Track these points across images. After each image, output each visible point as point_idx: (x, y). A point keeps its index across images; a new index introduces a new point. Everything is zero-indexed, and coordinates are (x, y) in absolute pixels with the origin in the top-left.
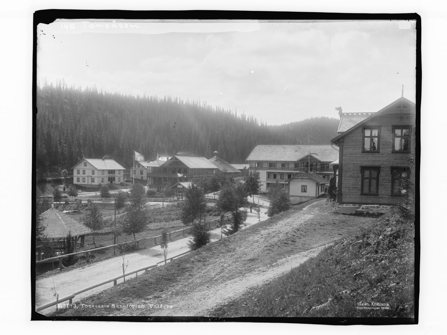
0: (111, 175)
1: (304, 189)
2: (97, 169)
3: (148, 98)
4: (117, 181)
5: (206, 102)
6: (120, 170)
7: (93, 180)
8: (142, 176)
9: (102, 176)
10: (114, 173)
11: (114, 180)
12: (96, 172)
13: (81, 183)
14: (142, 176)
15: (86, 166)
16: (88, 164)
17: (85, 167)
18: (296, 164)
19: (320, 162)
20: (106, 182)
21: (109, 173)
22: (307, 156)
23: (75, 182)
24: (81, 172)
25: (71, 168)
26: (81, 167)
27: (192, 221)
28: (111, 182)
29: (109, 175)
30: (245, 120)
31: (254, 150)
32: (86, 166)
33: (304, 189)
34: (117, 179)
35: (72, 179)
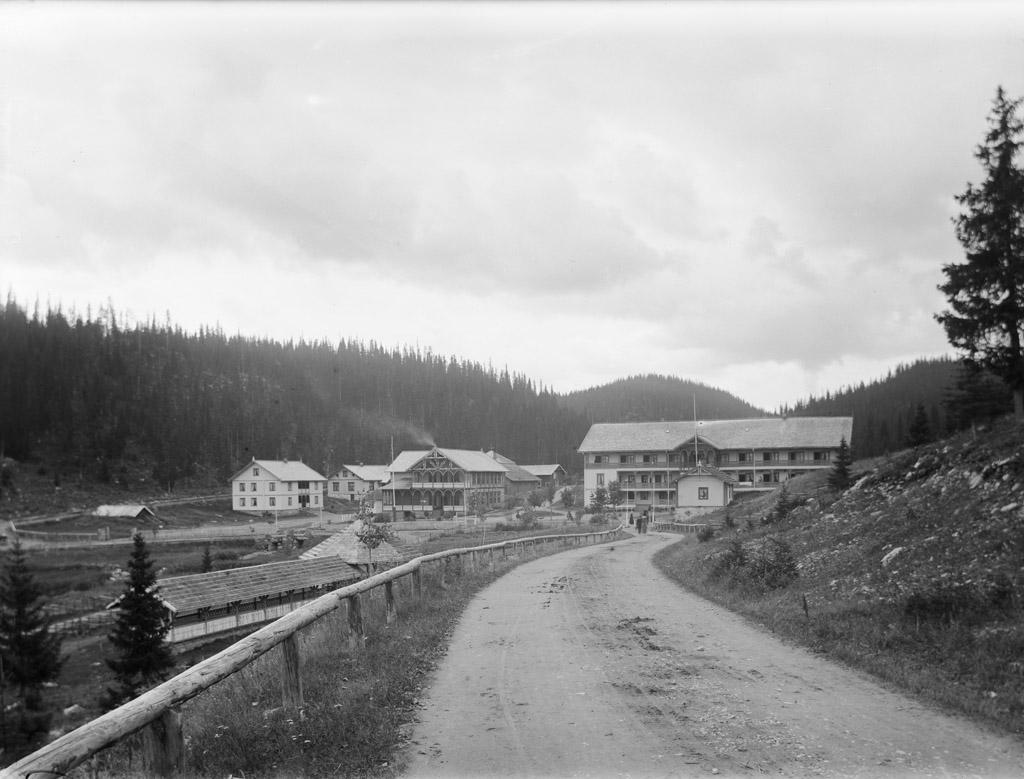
0: (304, 491)
1: (704, 494)
2: (279, 480)
3: (310, 346)
4: (312, 504)
5: (430, 348)
6: (316, 482)
7: (273, 502)
8: (352, 493)
9: (289, 493)
10: (308, 487)
11: (308, 501)
12: (278, 485)
13: (249, 507)
14: (352, 493)
15: (257, 474)
16: (261, 472)
17: (257, 478)
18: (671, 455)
19: (716, 450)
20: (296, 505)
21: (300, 487)
22: (693, 440)
23: (236, 506)
24: (248, 487)
25: (229, 480)
26: (247, 477)
27: (979, 287)
28: (304, 506)
29: (300, 491)
30: (181, 336)
31: (590, 433)
32: (257, 474)
33: (704, 494)
34: (312, 499)
35: (230, 501)
